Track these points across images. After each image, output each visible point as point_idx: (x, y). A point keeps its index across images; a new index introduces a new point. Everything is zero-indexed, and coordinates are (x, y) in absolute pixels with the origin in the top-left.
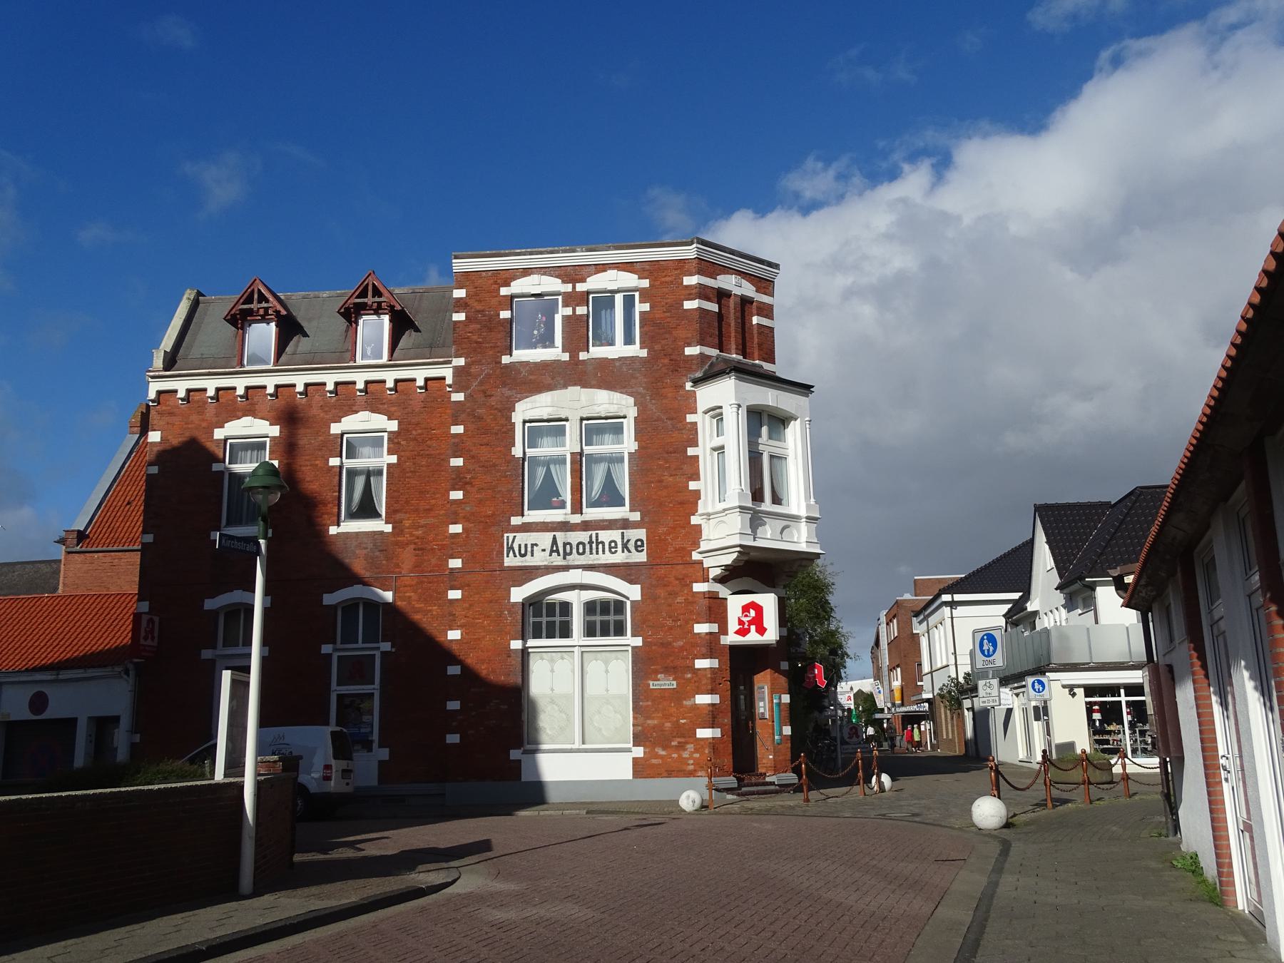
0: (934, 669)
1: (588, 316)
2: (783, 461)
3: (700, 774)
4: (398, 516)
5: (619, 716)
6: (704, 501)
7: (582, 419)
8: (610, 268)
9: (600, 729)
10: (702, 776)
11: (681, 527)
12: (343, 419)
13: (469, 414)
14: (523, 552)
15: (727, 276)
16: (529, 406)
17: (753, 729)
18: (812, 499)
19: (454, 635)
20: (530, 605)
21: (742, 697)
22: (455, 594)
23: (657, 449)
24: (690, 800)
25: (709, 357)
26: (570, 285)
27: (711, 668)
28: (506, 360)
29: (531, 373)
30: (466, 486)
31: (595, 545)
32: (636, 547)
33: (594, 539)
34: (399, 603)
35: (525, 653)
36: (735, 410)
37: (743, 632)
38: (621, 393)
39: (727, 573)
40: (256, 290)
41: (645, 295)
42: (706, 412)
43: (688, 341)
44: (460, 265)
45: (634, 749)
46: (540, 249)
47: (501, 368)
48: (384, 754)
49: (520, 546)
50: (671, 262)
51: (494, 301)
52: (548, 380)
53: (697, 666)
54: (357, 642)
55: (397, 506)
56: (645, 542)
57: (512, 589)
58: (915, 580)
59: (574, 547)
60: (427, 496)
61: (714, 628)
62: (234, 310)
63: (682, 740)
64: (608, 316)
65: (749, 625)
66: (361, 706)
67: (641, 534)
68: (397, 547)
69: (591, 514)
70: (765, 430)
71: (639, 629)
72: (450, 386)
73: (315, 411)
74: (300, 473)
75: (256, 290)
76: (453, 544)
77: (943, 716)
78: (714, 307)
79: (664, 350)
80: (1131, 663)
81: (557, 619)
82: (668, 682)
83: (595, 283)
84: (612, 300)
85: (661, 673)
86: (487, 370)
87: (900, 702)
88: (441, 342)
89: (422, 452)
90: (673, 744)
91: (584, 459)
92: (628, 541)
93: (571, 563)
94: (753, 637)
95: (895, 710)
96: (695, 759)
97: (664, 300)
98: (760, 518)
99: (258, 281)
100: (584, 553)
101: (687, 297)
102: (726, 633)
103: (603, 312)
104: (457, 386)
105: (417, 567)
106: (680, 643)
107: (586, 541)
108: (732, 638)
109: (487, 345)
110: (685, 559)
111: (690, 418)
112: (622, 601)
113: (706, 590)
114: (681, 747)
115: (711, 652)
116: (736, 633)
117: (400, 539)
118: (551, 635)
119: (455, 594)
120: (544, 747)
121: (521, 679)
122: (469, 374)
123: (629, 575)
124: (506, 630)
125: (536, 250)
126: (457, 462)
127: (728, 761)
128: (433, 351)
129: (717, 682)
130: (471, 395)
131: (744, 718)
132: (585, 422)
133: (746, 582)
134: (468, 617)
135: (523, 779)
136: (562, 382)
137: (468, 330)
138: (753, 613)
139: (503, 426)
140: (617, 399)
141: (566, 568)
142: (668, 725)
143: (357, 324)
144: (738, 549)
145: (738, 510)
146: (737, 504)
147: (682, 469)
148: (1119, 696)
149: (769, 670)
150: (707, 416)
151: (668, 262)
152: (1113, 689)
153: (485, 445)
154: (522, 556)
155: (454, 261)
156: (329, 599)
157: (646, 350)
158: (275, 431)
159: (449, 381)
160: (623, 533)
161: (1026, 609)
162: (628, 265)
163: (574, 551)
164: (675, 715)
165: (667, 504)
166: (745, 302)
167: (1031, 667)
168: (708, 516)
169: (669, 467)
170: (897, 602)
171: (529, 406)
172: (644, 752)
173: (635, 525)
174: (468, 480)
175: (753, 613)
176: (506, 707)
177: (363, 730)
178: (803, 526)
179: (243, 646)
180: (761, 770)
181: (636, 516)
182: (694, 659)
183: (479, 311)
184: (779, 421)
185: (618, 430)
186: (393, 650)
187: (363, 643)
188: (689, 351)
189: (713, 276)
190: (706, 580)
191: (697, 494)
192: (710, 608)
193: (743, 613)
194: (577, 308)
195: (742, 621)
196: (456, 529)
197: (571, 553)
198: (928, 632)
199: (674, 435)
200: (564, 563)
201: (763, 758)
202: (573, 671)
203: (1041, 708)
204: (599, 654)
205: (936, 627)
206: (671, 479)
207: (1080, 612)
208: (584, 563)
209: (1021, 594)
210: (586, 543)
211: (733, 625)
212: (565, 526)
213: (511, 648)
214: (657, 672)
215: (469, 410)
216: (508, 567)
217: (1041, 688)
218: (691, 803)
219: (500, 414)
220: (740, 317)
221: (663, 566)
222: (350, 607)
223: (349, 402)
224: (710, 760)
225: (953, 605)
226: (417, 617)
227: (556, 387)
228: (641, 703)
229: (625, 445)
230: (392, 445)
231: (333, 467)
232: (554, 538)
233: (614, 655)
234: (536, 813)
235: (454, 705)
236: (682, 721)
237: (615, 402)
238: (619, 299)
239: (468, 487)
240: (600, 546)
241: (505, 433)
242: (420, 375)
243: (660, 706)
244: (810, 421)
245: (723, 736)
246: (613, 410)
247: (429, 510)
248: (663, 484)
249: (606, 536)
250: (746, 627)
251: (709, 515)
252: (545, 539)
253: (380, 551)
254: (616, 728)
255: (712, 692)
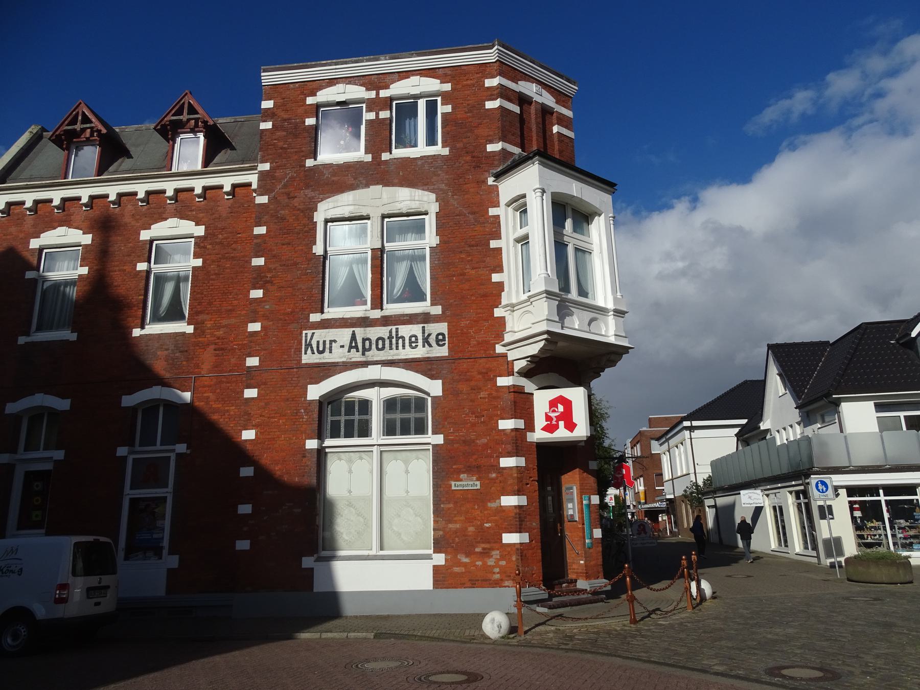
0: (674, 477)
1: (391, 119)
2: (587, 255)
3: (506, 583)
4: (201, 317)
5: (419, 519)
6: (507, 292)
7: (384, 217)
8: (413, 75)
9: (400, 534)
10: (509, 587)
11: (485, 320)
12: (153, 227)
13: (272, 216)
14: (321, 349)
15: (527, 83)
16: (331, 205)
17: (562, 531)
18: (619, 294)
19: (248, 435)
20: (329, 403)
21: (550, 498)
22: (251, 393)
23: (459, 242)
24: (495, 625)
25: (512, 154)
26: (381, 117)
27: (517, 467)
28: (310, 163)
29: (334, 174)
30: (267, 285)
31: (395, 340)
32: (437, 341)
33: (394, 334)
34: (197, 404)
35: (321, 453)
36: (539, 194)
37: (550, 428)
38: (423, 190)
39: (533, 366)
40: (80, 113)
41: (447, 97)
42: (508, 205)
43: (489, 138)
44: (269, 78)
45: (435, 556)
46: (345, 60)
47: (305, 171)
48: (173, 561)
49: (318, 342)
50: (472, 67)
51: (300, 110)
52: (351, 181)
53: (502, 465)
54: (155, 445)
55: (199, 308)
56: (447, 336)
57: (309, 386)
58: (650, 418)
59: (374, 342)
60: (230, 297)
61: (520, 424)
62: (59, 131)
63: (487, 546)
64: (413, 123)
65: (557, 421)
66: (156, 510)
67: (443, 327)
68: (197, 348)
69: (391, 309)
70: (569, 224)
71: (441, 426)
72: (255, 191)
73: (127, 219)
74: (109, 278)
75: (80, 113)
76: (251, 342)
77: (684, 512)
78: (516, 109)
79: (465, 148)
80: (888, 466)
81: (356, 417)
82: (472, 483)
83: (399, 88)
84: (415, 105)
85: (464, 473)
86: (290, 173)
87: (644, 501)
88: (253, 156)
89: (227, 255)
90: (477, 550)
91: (385, 255)
92: (429, 335)
93: (370, 359)
94: (562, 433)
95: (641, 506)
96: (500, 567)
97: (466, 102)
98: (567, 307)
99: (83, 104)
100: (383, 348)
101: (488, 98)
102: (533, 430)
103: (407, 122)
104: (262, 190)
105: (216, 367)
106: (484, 441)
107: (386, 335)
108: (539, 435)
109: (292, 150)
110: (488, 352)
111: (492, 212)
112: (424, 398)
113: (511, 383)
114: (486, 553)
115: (517, 449)
116: (543, 429)
117: (200, 339)
118: (349, 435)
119: (251, 393)
120: (342, 553)
121: (315, 481)
122: (274, 177)
123: (430, 370)
124: (302, 429)
125: (342, 60)
126: (259, 262)
127: (537, 569)
128: (247, 161)
129: (525, 481)
130: (275, 198)
131: (552, 520)
132: (386, 220)
133: (553, 377)
134: (263, 416)
135: (317, 589)
136: (364, 182)
137: (274, 137)
138: (561, 408)
139: (305, 225)
140: (419, 195)
141: (365, 364)
142: (471, 529)
143: (174, 142)
144: (545, 336)
145: (545, 295)
146: (543, 289)
147: (485, 262)
148: (879, 495)
149: (578, 469)
150: (510, 209)
151: (469, 67)
152: (872, 490)
153: (287, 244)
154: (320, 352)
155: (262, 74)
156: (128, 401)
157: (448, 149)
158: (87, 239)
159: (254, 186)
160: (423, 327)
161: (760, 428)
162: (430, 71)
163: (374, 346)
164: (479, 518)
165: (469, 297)
166: (546, 111)
167: (785, 470)
168: (512, 307)
169: (472, 260)
170: (640, 432)
171: (331, 205)
172: (445, 559)
173: (437, 319)
174: (268, 279)
175: (561, 408)
176: (299, 510)
177: (155, 536)
178: (611, 319)
179: (44, 450)
180: (572, 576)
181: (437, 310)
182: (498, 457)
183: (285, 120)
184: (584, 217)
185: (419, 229)
186: (189, 452)
187: (161, 445)
188: (490, 148)
189: (515, 80)
190: (510, 373)
191: (500, 286)
192: (515, 402)
193: (550, 410)
194: (380, 113)
195: (550, 416)
196: (255, 327)
197: (370, 349)
198: (669, 451)
199: (476, 229)
200: (363, 359)
201: (574, 563)
202: (372, 472)
203: (826, 507)
204: (398, 454)
205: (677, 447)
206: (473, 272)
207: (819, 426)
208: (384, 358)
209: (746, 421)
210: (386, 338)
211: (540, 421)
212: (364, 322)
213: (306, 448)
214: (459, 472)
215: (272, 212)
216: (306, 364)
217: (824, 489)
218: (497, 629)
219: (302, 214)
220: (541, 122)
221: (465, 361)
222: (151, 407)
223: (160, 211)
224: (519, 574)
225: (691, 429)
226: (215, 417)
227: (359, 186)
228: (442, 506)
229: (427, 241)
230: (198, 249)
231: (140, 271)
232: (354, 334)
233: (414, 454)
234: (317, 635)
235: (245, 509)
236: (487, 525)
237: (416, 198)
238: (422, 105)
239: (269, 286)
240: (400, 341)
241: (306, 232)
242: (227, 182)
243: (462, 509)
244: (614, 217)
245: (531, 540)
246: (414, 206)
247: (231, 310)
248: (466, 277)
249: (406, 330)
250: (554, 422)
251: (513, 306)
252: (343, 335)
253: (180, 352)
254: (416, 533)
255: (518, 493)
